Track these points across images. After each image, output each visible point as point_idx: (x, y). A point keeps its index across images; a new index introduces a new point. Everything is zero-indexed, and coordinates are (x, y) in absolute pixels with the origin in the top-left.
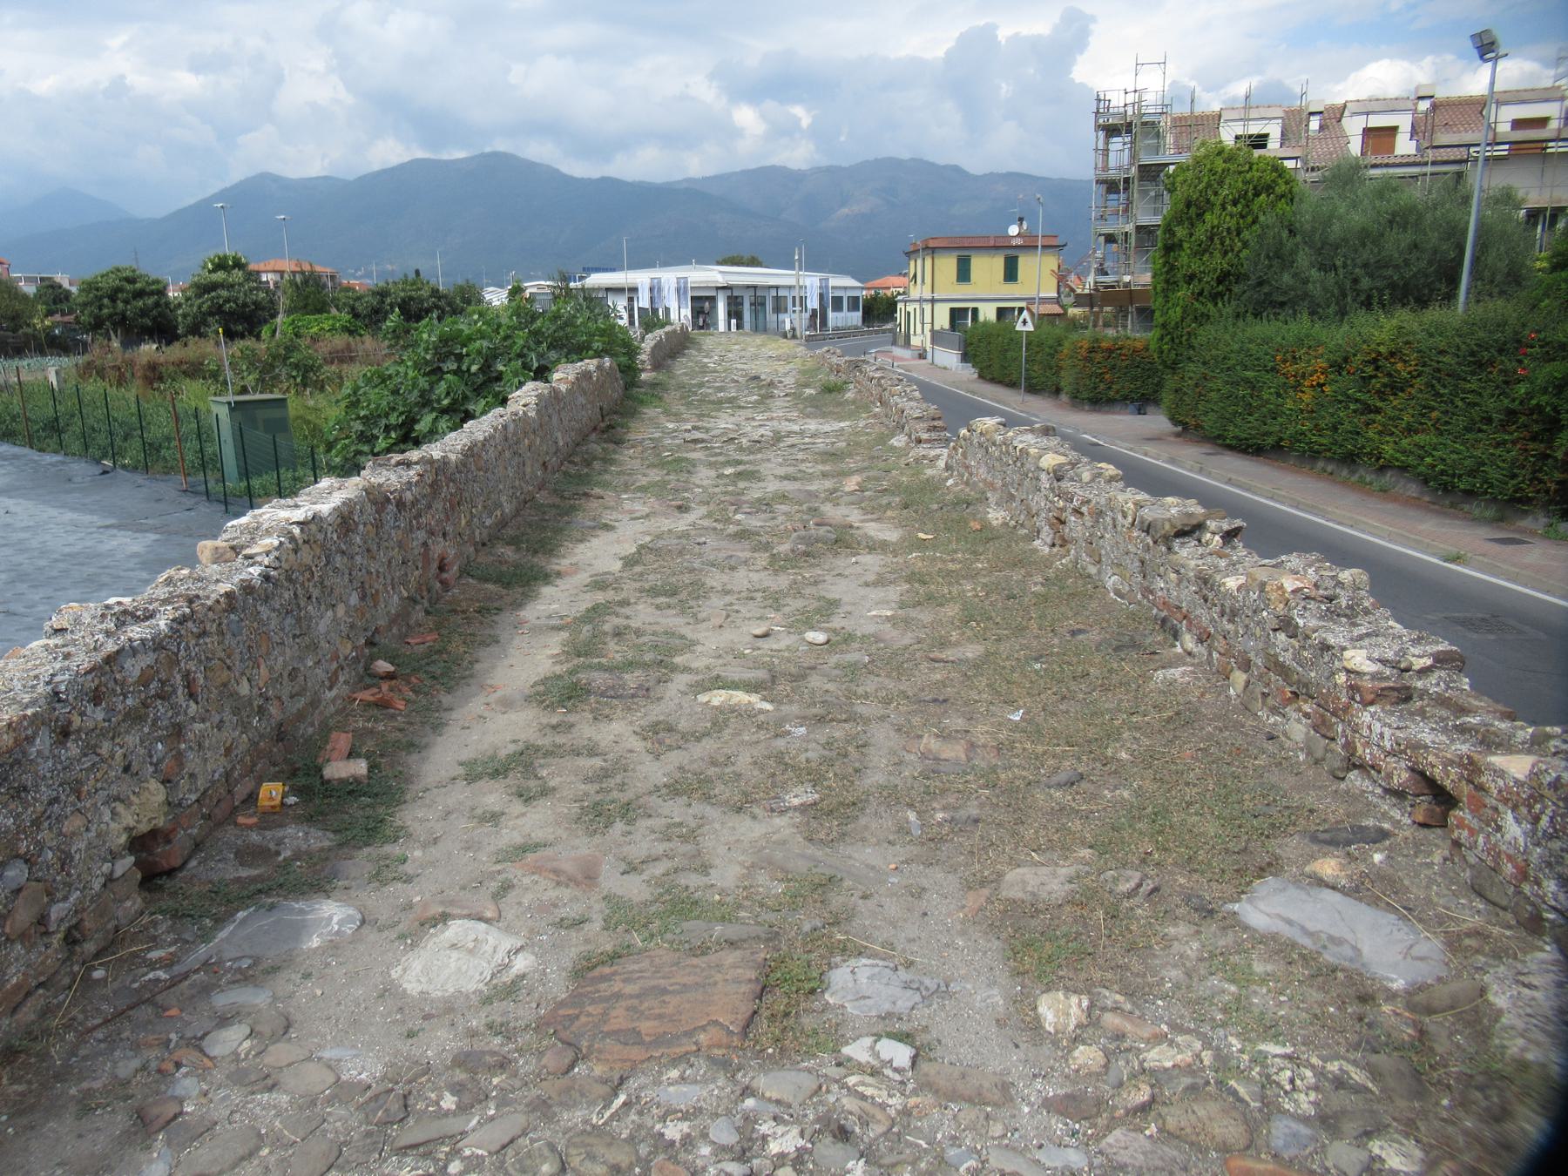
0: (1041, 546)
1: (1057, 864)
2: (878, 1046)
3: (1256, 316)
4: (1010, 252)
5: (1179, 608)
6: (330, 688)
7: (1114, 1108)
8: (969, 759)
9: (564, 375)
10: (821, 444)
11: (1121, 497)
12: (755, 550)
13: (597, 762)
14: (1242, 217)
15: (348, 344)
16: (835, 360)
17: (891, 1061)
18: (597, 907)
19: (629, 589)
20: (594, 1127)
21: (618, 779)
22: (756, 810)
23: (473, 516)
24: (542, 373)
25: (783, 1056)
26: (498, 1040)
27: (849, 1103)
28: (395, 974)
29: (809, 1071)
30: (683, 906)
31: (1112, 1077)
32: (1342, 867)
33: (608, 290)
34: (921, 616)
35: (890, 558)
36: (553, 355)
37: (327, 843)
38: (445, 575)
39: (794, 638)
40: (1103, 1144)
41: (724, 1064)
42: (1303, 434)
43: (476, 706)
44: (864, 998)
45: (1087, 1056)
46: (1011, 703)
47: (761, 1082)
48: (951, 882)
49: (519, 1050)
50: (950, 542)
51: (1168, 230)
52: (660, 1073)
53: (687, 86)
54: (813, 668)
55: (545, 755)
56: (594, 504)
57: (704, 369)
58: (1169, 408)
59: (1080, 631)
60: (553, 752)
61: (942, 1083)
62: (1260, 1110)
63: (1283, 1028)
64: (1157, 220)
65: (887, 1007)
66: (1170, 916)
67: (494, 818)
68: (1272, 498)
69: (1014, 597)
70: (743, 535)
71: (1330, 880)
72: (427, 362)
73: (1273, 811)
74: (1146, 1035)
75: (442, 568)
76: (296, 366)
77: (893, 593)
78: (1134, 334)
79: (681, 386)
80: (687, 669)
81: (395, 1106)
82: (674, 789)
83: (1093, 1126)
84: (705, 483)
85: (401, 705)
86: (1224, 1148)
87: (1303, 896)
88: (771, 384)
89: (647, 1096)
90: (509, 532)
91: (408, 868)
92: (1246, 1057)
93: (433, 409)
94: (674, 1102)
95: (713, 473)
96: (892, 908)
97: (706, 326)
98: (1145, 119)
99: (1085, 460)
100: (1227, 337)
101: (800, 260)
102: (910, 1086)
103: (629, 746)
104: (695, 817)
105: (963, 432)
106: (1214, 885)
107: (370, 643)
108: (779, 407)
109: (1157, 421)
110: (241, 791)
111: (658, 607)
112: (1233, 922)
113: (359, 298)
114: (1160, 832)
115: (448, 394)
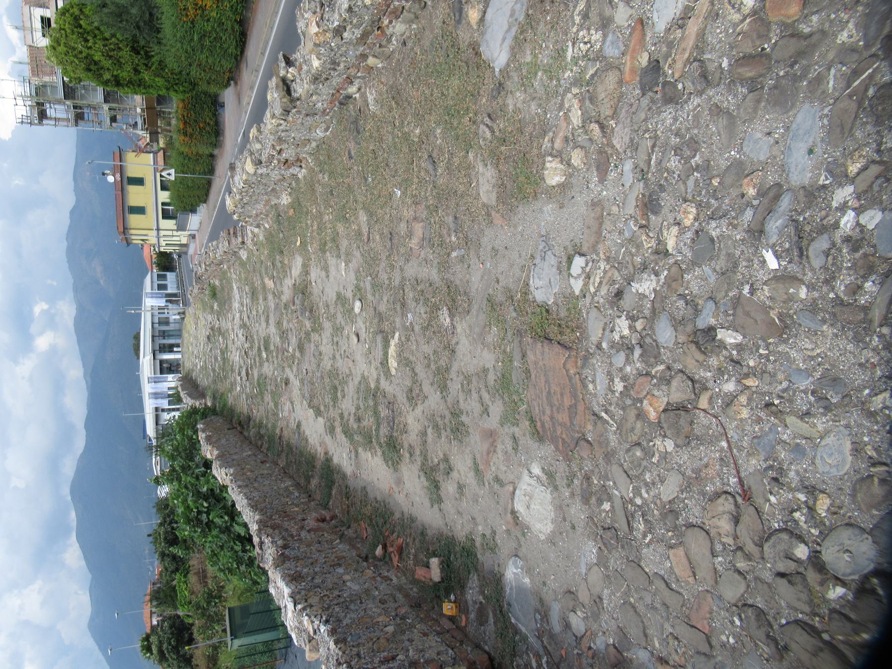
0: (302, 174)
1: (477, 172)
2: (575, 275)
3: (159, 32)
4: (125, 180)
5: (333, 95)
6: (391, 580)
7: (602, 143)
8: (422, 221)
9: (208, 452)
10: (247, 301)
11: (269, 127)
12: (310, 341)
13: (430, 431)
14: (95, 36)
15: (195, 574)
16: (196, 291)
17: (582, 268)
18: (507, 430)
19: (334, 413)
20: (618, 429)
21: (438, 419)
22: (453, 342)
23: (293, 504)
24: (207, 465)
25: (581, 327)
26: (576, 481)
27: (604, 291)
28: (543, 537)
29: (588, 313)
30: (505, 383)
31: (587, 144)
32: (473, 7)
33: (157, 424)
34: (345, 246)
35: (312, 263)
36: (197, 459)
37: (476, 577)
38: (328, 518)
39: (358, 320)
40: (620, 150)
41: (586, 359)
42: (232, 7)
43: (400, 498)
44: (550, 282)
45: (577, 158)
46: (391, 195)
47: (594, 339)
48: (489, 232)
49: (581, 470)
50: (301, 227)
51: (106, 83)
52: (591, 394)
53: (23, 378)
54: (375, 309)
55: (426, 460)
56: (285, 433)
57: (204, 368)
58: (220, 88)
59: (349, 153)
60: (425, 456)
61: (592, 239)
62: (601, 62)
63: (558, 47)
64: (100, 90)
65: (554, 270)
66: (503, 108)
67: (461, 487)
68: (272, 28)
69: (332, 191)
70: (301, 347)
71: (481, 14)
72: (203, 531)
73: (445, 45)
74: (565, 125)
75: (323, 520)
76: (209, 603)
77: (332, 261)
78: (174, 106)
79: (215, 382)
80: (378, 381)
81: (609, 534)
82: (443, 388)
83: (612, 155)
84: (272, 369)
85: (401, 540)
86: (621, 82)
87: (490, 30)
88: (212, 329)
89: (602, 401)
90: (302, 482)
91: (488, 533)
92: (575, 68)
93: (231, 525)
94: (604, 386)
95: (266, 364)
96: (503, 266)
97: (178, 365)
98: (34, 93)
99: (248, 146)
100: (173, 50)
101: (134, 310)
102: (595, 257)
103: (421, 413)
104: (458, 376)
105: (235, 217)
106: (486, 82)
107: (366, 559)
108: (226, 325)
109: (228, 96)
110: (447, 625)
111: (344, 397)
112: (505, 71)
113: (166, 569)
114: (459, 112)
115: (222, 517)
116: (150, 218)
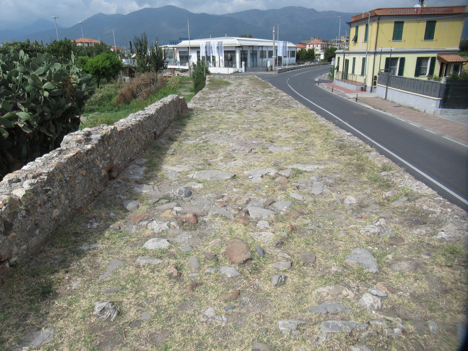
116: (387, 44)
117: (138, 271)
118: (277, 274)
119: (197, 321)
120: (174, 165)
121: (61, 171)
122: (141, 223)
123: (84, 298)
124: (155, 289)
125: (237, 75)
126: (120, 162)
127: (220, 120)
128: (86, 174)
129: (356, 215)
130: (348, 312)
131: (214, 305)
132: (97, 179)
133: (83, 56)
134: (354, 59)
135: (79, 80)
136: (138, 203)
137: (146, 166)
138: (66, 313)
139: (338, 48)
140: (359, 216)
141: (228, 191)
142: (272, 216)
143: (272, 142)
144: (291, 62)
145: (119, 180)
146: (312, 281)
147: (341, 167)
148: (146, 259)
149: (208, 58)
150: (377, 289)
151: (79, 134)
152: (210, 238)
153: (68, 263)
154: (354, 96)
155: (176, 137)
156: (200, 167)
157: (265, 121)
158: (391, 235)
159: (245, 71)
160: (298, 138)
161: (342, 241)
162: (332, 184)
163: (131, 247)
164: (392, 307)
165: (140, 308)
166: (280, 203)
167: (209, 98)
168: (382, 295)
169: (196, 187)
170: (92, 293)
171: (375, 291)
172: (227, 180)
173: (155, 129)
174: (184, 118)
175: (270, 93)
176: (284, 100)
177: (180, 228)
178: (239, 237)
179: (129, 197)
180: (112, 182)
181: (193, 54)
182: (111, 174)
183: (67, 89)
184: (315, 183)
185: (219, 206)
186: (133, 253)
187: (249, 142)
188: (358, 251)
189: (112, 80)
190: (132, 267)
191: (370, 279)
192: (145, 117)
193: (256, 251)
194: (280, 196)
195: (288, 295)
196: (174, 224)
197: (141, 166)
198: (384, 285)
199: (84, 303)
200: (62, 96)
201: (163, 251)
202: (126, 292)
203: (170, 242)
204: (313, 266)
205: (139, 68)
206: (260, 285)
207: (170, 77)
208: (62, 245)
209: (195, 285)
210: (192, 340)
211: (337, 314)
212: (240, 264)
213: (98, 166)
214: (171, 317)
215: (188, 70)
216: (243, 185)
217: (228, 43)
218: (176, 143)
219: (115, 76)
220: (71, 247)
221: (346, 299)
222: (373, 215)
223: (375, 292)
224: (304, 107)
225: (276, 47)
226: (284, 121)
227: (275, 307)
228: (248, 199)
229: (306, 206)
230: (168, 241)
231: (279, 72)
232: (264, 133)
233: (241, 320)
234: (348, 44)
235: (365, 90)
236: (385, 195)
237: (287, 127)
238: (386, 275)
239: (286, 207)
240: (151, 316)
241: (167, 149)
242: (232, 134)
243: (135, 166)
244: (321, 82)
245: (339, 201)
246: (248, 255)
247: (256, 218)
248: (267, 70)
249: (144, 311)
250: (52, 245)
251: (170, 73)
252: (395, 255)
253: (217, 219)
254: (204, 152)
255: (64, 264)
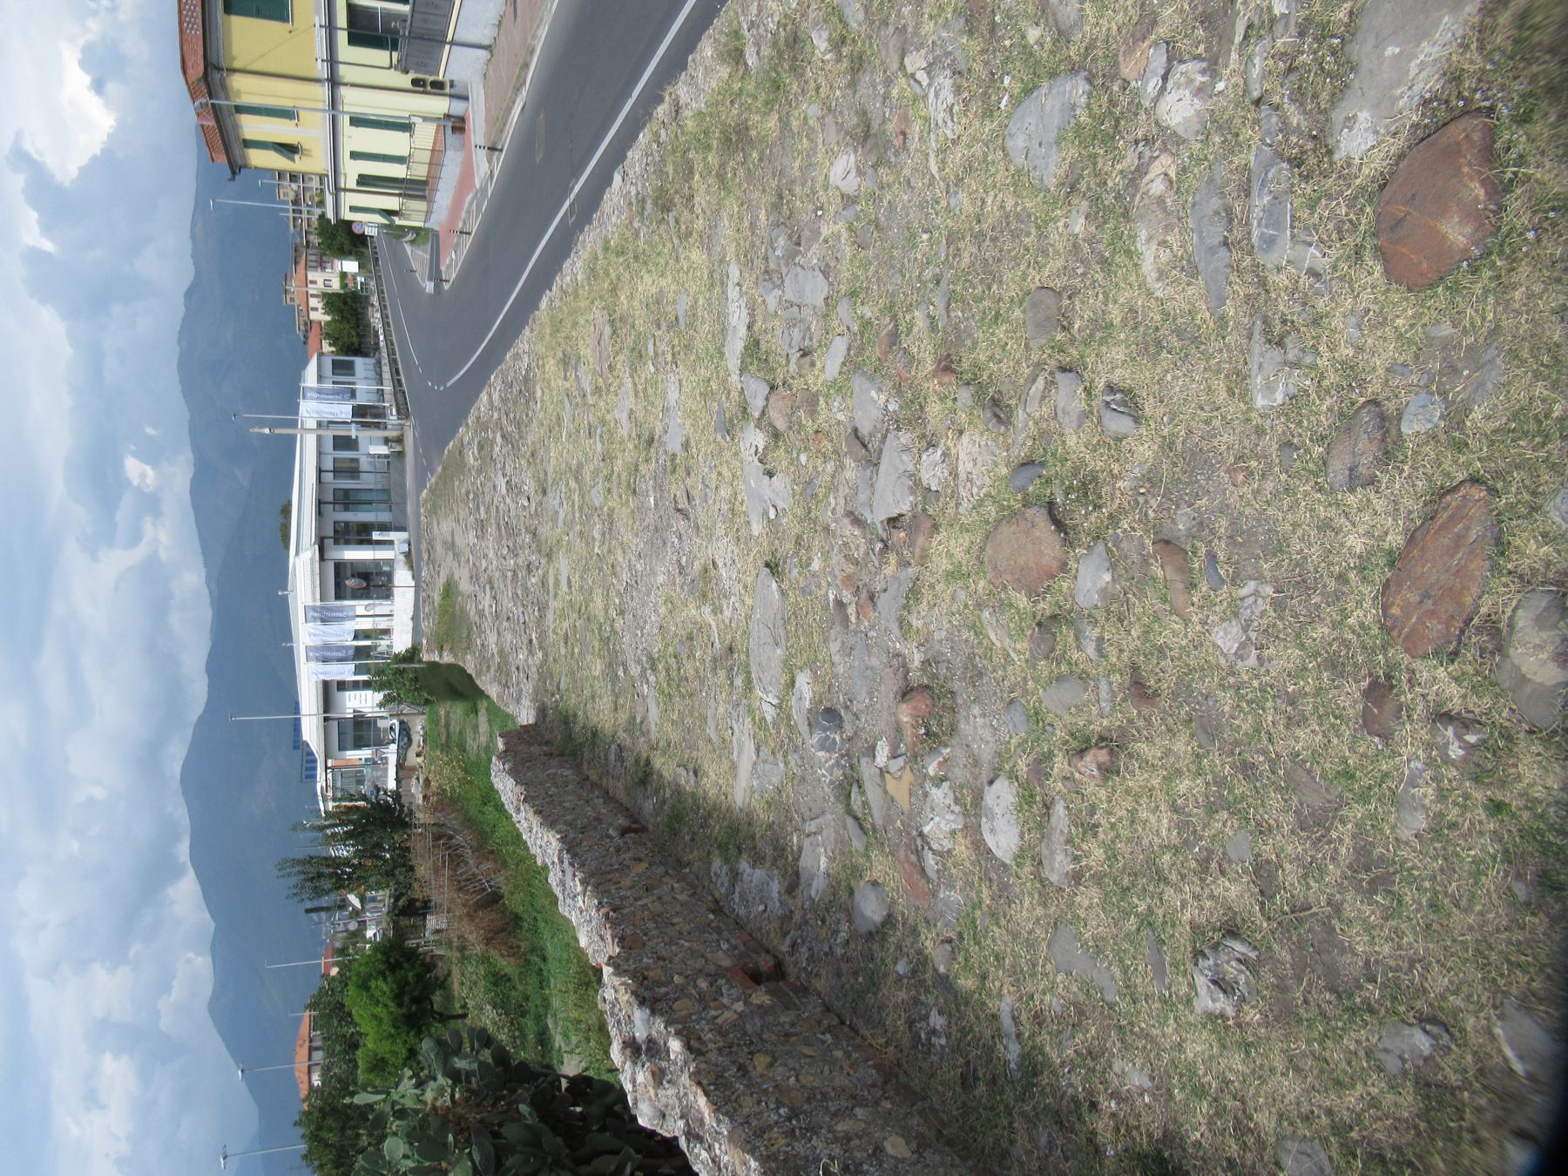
117: (1092, 876)
118: (1100, 422)
119: (1257, 677)
120: (734, 767)
121: (760, 1133)
122: (932, 874)
123: (1179, 1047)
124: (1153, 819)
125: (420, 558)
126: (725, 946)
127: (575, 615)
128: (766, 1052)
129: (897, 154)
130: (1221, 171)
131: (1203, 623)
132: (783, 1019)
133: (356, 1066)
134: (355, 155)
135: (442, 1080)
136: (862, 883)
137: (738, 858)
138: (1231, 1104)
139: (318, 211)
140: (897, 142)
141: (819, 586)
142: (905, 437)
143: (651, 441)
144: (372, 374)
145: (785, 948)
146: (1122, 300)
147: (732, 205)
148: (1052, 853)
149: (360, 653)
150: (1142, 76)
151: (634, 1080)
152: (980, 643)
153: (1064, 1103)
154: (480, 158)
155: (637, 761)
156: (739, 682)
157: (580, 466)
158: (962, 32)
159: (403, 529)
160: (636, 353)
161: (983, 201)
162: (790, 237)
163: (1010, 902)
164: (1202, 22)
165: (1214, 865)
166: (859, 414)
167: (501, 652)
168: (1164, 59)
169: (808, 695)
170: (1164, 1024)
171: (1152, 84)
172: (783, 593)
173: (611, 832)
174: (569, 737)
175: (481, 447)
176: (504, 401)
177: (946, 746)
178: (975, 548)
179: (842, 916)
180: (791, 970)
181: (348, 704)
182: (764, 973)
183: (473, 1117)
184: (789, 295)
185: (873, 615)
186: (1030, 894)
187: (651, 519)
188: (1017, 143)
189: (440, 970)
190: (1078, 899)
191: (1110, 101)
192: (571, 864)
193: (1023, 489)
194: (835, 413)
195: (1169, 377)
196: (935, 764)
197: (735, 875)
198: (1130, 51)
199: (1197, 1047)
200: (496, 1135)
201: (1026, 798)
202: (1160, 912)
203: (997, 776)
204: (1070, 298)
205: (398, 883)
206: (1137, 472)
207: (427, 782)
208: (1006, 1122)
209: (1140, 690)
210: (1319, 692)
211: (1229, 210)
212: (1069, 543)
213: (741, 1015)
214: (1244, 764)
215: (401, 723)
216: (799, 538)
217: (309, 582)
218: (657, 763)
219: (423, 964)
220: (1009, 1096)
221: (1179, 181)
222: (895, 92)
223: (1153, 84)
224: (527, 332)
225: (319, 424)
226: (579, 400)
227: (1207, 422)
228: (846, 521)
229: (869, 323)
230: (991, 782)
231: (407, 417)
232: (618, 466)
233: (1251, 533)
234: (305, 177)
235: (462, 119)
236: (824, 54)
237: (597, 390)
238: (1096, 47)
239: (873, 394)
240: (1240, 828)
241: (678, 792)
242: (625, 576)
243: (736, 897)
244: (439, 272)
245: (850, 213)
246: (1039, 516)
247: (913, 493)
248: (401, 454)
249: (1224, 853)
250: (1004, 1157)
251: (414, 781)
252: (1026, 16)
253: (917, 623)
254: (689, 668)
255: (1069, 1115)
